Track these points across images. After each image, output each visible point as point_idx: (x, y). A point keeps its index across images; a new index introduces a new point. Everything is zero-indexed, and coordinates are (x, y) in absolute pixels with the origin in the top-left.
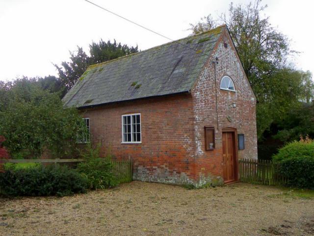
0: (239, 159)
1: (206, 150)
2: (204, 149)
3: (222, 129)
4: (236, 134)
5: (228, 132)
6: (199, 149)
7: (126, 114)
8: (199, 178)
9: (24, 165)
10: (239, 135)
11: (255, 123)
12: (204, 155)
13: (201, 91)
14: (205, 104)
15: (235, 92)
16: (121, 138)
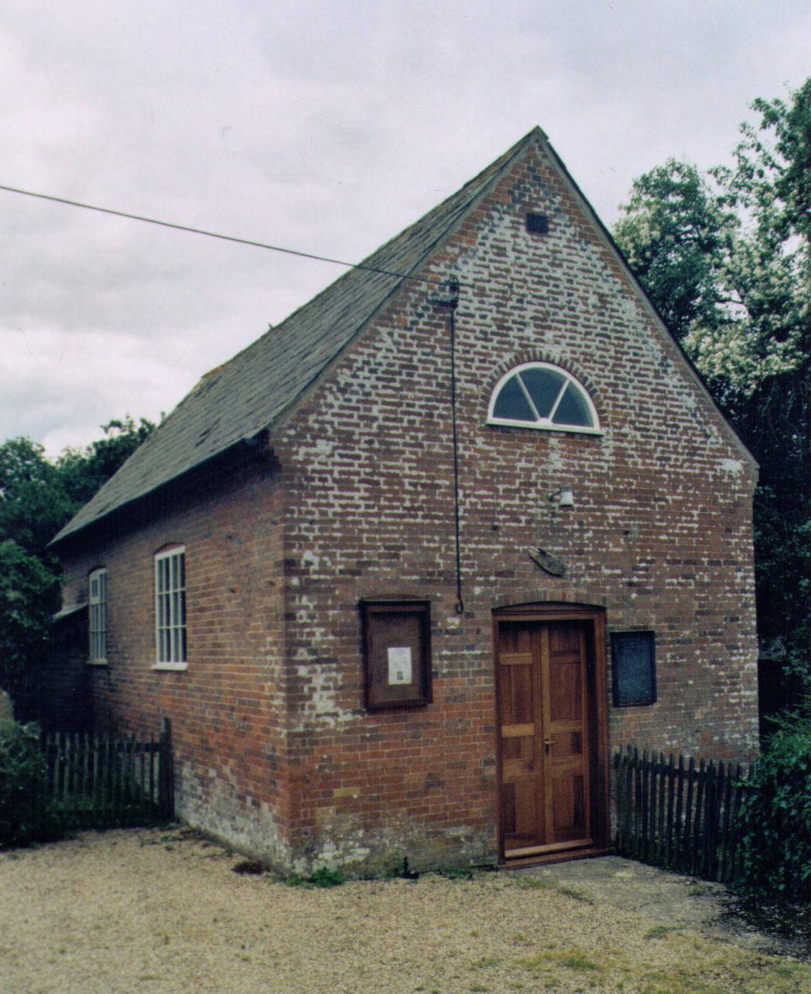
0: (615, 749)
1: (371, 707)
2: (358, 704)
3: (495, 612)
4: (598, 632)
5: (551, 625)
6: (323, 703)
7: (164, 547)
8: (316, 834)
9: (610, 679)
10: (616, 637)
11: (745, 578)
12: (352, 729)
13: (346, 439)
14: (375, 493)
15: (599, 436)
16: (154, 646)
